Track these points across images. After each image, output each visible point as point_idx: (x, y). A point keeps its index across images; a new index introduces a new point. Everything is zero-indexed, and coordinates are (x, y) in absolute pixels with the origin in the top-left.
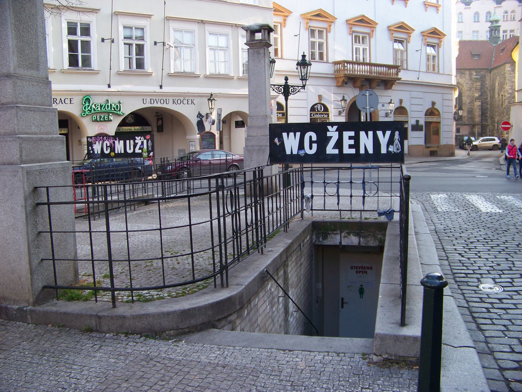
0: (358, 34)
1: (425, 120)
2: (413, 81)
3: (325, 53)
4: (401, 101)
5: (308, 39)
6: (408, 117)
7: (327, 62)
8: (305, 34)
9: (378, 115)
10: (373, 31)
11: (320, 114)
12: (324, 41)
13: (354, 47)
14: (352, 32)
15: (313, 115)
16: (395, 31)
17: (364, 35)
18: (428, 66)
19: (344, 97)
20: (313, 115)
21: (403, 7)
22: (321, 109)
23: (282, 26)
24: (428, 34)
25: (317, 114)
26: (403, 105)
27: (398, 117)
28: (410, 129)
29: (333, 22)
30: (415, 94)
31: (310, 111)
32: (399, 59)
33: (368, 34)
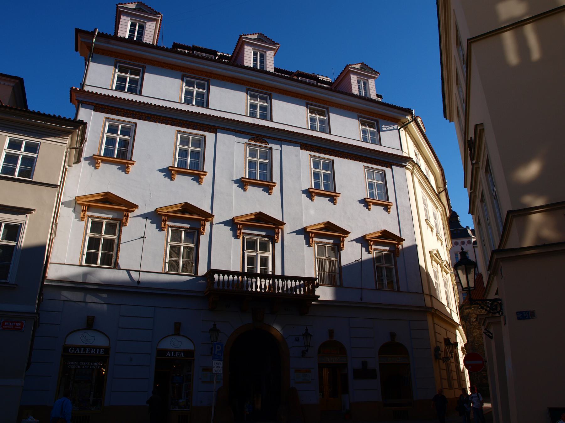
4: (331, 333)
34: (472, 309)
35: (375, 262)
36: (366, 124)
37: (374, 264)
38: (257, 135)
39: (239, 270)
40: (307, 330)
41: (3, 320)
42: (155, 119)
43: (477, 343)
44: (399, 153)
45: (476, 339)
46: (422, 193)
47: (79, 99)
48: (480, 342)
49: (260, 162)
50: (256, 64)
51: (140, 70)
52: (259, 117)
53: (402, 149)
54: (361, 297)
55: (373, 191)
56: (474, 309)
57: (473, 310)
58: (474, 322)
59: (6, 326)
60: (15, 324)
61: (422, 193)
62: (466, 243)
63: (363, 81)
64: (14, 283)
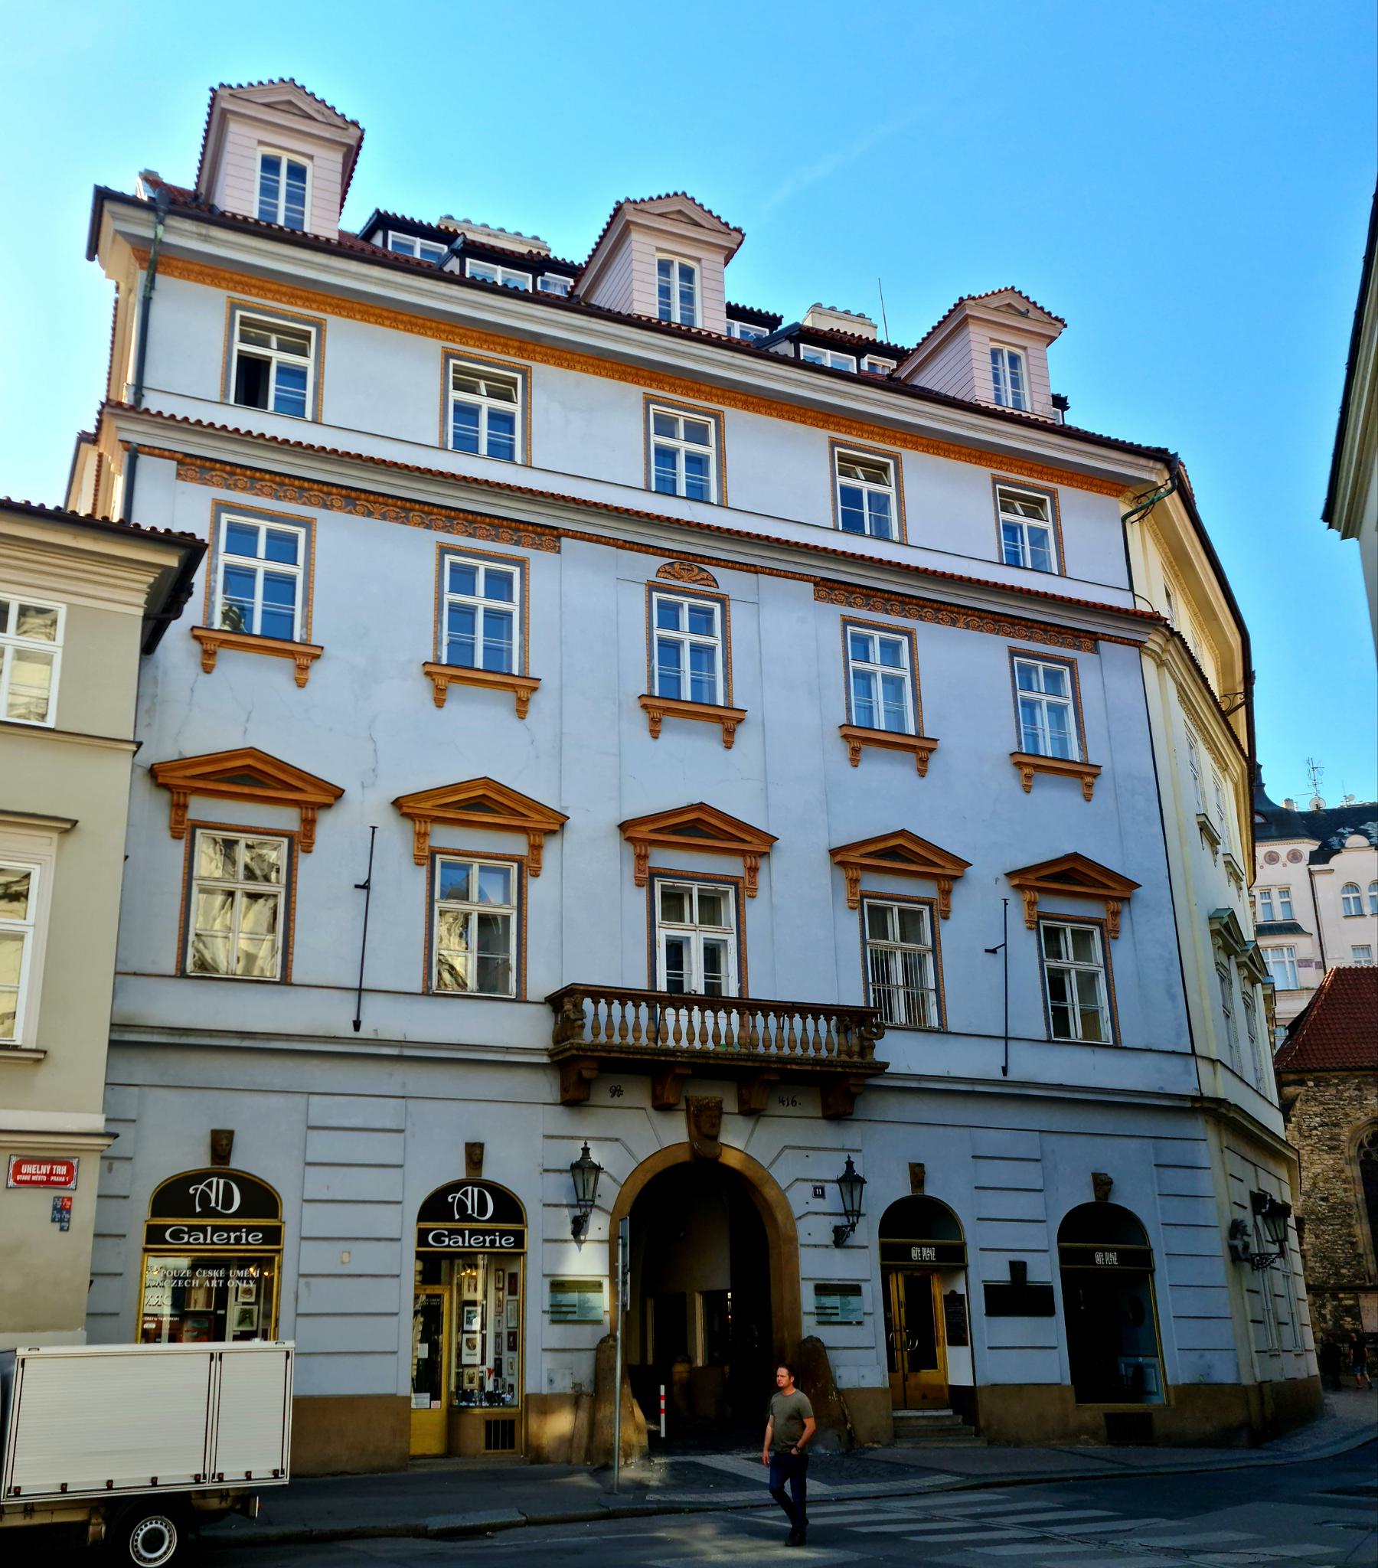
2: (508, 1050)
4: (917, 1174)
5: (1037, 960)
7: (521, 999)
8: (1026, 947)
9: (793, 1240)
13: (662, 935)
14: (647, 877)
15: (437, 1238)
20: (438, 1238)
22: (483, 1209)
23: (527, 873)
24: (1038, 879)
26: (929, 1191)
28: (977, 1303)
29: (765, 854)
31: (422, 1217)
33: (735, 882)
34: (1307, 1086)
35: (1044, 956)
36: (1017, 504)
37: (1042, 962)
39: (641, 983)
40: (850, 1164)
41: (14, 1160)
42: (369, 506)
43: (1323, 1199)
45: (1321, 1184)
46: (1214, 771)
47: (130, 439)
48: (1335, 1194)
49: (244, 320)
50: (669, 305)
52: (684, 494)
54: (1004, 1065)
55: (1035, 729)
56: (1315, 1086)
57: (1311, 1087)
58: (1315, 1128)
59: (26, 1174)
60: (52, 1169)
61: (1214, 771)
64: (34, 1046)
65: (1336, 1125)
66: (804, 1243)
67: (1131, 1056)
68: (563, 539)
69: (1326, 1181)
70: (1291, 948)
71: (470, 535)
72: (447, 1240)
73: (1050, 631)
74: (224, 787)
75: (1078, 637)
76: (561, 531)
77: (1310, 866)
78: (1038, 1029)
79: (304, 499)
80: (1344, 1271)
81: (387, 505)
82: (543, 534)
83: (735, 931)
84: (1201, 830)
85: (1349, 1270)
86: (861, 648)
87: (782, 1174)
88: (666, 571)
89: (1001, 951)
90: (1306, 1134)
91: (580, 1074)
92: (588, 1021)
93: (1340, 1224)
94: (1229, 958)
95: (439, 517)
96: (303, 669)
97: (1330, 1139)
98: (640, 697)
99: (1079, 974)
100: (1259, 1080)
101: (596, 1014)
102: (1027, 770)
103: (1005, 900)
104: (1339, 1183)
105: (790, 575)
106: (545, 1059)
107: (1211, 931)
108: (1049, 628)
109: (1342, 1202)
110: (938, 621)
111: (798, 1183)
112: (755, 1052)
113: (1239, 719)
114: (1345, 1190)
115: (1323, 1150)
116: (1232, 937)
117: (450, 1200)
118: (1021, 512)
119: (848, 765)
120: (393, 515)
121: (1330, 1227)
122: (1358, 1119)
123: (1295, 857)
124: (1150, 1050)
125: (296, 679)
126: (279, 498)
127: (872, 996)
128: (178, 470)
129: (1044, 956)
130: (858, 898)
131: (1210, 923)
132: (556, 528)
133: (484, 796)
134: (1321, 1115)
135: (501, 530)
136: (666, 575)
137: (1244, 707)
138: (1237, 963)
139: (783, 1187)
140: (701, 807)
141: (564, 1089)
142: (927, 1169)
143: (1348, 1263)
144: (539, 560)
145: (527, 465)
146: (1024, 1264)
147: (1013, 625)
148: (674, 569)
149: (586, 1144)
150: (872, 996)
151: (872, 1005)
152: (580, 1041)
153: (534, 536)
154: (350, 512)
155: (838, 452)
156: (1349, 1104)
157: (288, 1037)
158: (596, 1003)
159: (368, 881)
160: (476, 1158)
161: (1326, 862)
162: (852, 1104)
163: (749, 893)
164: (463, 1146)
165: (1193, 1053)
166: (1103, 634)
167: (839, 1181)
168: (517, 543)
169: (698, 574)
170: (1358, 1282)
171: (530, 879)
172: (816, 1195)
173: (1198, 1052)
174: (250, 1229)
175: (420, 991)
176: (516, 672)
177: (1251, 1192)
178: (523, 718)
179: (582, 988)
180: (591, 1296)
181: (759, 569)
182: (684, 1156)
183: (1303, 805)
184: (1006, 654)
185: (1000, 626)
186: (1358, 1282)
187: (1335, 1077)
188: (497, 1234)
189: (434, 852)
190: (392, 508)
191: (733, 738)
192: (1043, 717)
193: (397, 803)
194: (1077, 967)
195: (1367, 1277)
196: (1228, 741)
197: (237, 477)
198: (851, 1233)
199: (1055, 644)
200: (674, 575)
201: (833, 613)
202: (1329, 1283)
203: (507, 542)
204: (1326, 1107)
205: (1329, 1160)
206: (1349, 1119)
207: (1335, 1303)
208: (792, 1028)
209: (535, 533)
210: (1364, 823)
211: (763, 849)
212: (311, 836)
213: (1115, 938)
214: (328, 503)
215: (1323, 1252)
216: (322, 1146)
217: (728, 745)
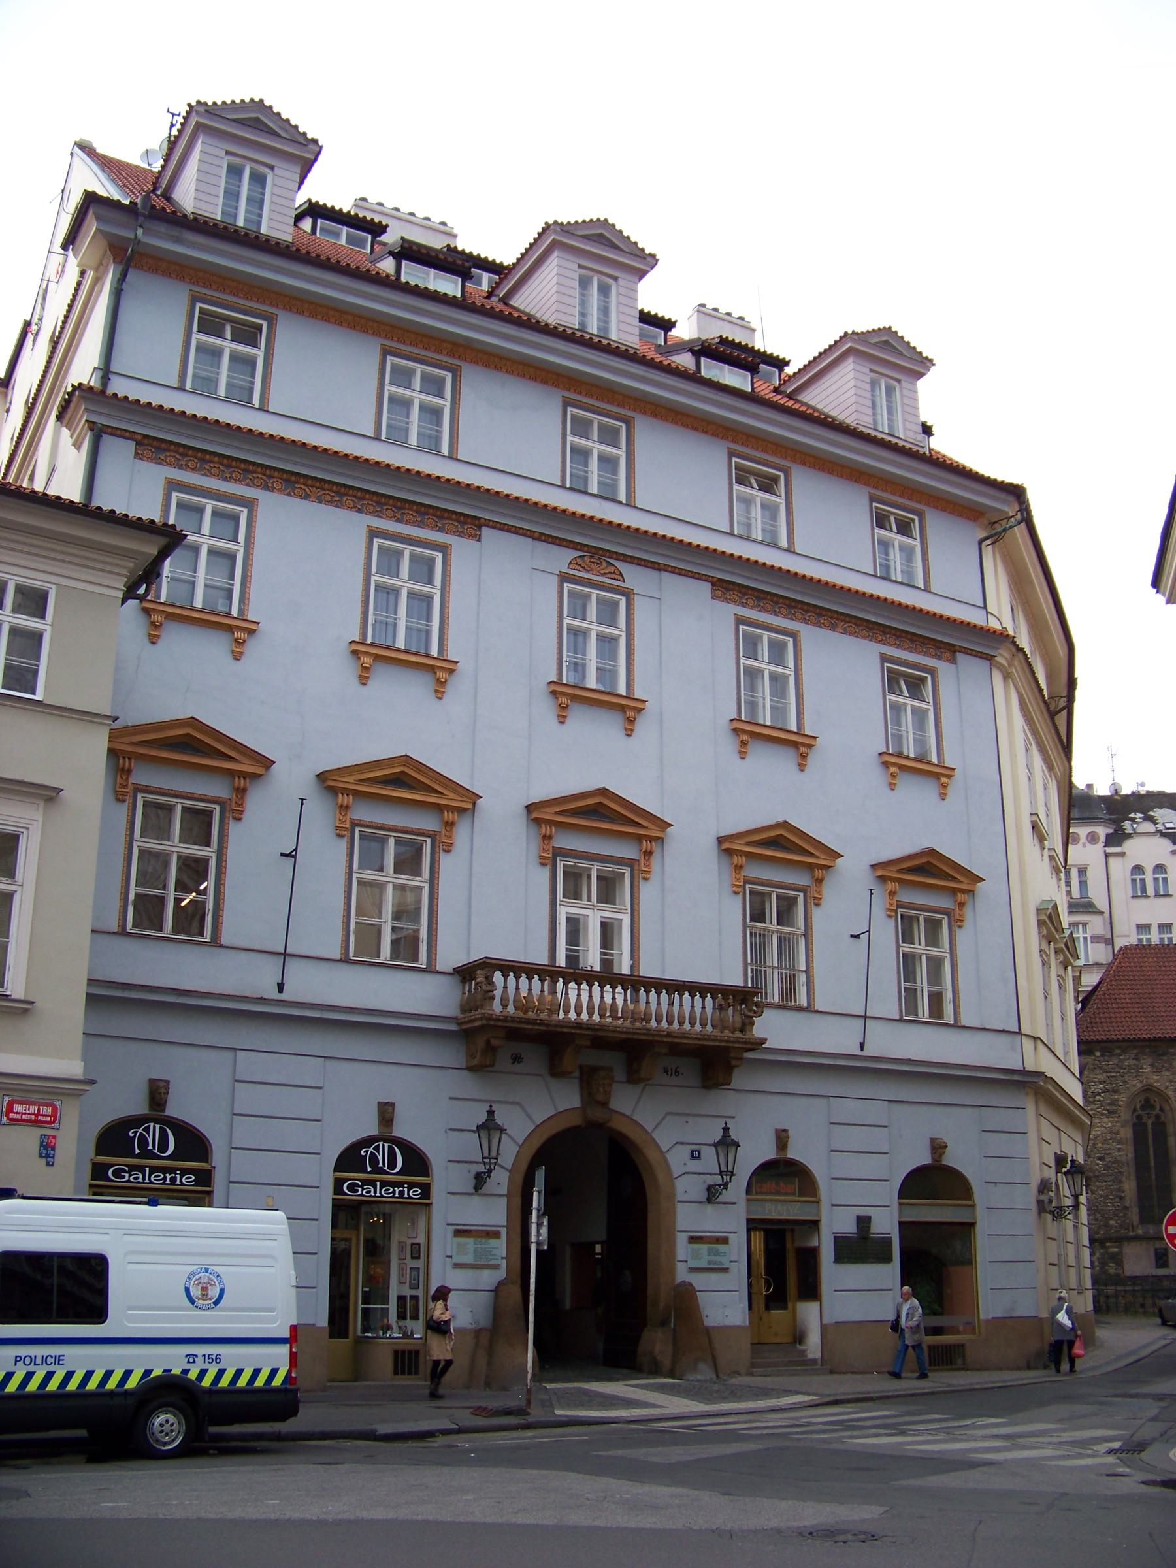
0: (582, 864)
1: (748, 1212)
3: (948, 995)
4: (782, 1139)
6: (818, 1202)
7: (431, 970)
8: (885, 932)
9: (671, 1197)
10: (648, 854)
11: (384, 1184)
12: (943, 951)
13: (562, 913)
14: (549, 859)
15: (352, 1188)
16: (357, 794)
17: (608, 867)
18: (910, 997)
19: (491, 1113)
20: (352, 1188)
21: (794, 768)
22: (392, 1164)
25: (372, 1183)
26: (792, 1154)
27: (768, 1205)
30: (847, 1109)
31: (338, 1167)
32: (773, 968)
33: (630, 863)
34: (1095, 1055)
37: (898, 946)
38: (593, 550)
39: (543, 959)
41: (7, 1099)
42: (307, 490)
43: (1100, 1159)
44: (975, 617)
45: (1100, 1145)
51: (262, 325)
53: (985, 607)
56: (1102, 1055)
58: (1099, 1094)
59: (17, 1113)
61: (1025, 732)
62: (1083, 839)
63: (885, 382)
65: (1115, 1092)
66: (680, 1199)
67: (967, 1034)
68: (484, 529)
69: (1105, 1142)
70: (1085, 925)
71: (398, 520)
72: (360, 1189)
73: (916, 641)
74: (165, 754)
75: (939, 648)
76: (482, 521)
77: (1106, 849)
78: (891, 1008)
79: (248, 480)
80: (1112, 1222)
81: (323, 489)
82: (465, 523)
83: (629, 911)
84: (1033, 828)
85: (1116, 1221)
86: (752, 645)
87: (664, 1138)
88: (577, 564)
89: (864, 937)
90: (1091, 1099)
91: (488, 1042)
92: (498, 994)
93: (1113, 1181)
94: (1049, 945)
95: (370, 502)
96: (240, 643)
97: (1110, 1104)
98: (549, 683)
99: (928, 958)
100: (1066, 1053)
101: (505, 987)
102: (893, 769)
103: (871, 890)
104: (1114, 1144)
105: (690, 574)
106: (453, 1027)
107: (1038, 921)
108: (915, 638)
109: (1116, 1161)
110: (820, 625)
111: (677, 1146)
112: (648, 1026)
113: (1061, 719)
114: (1119, 1150)
115: (1102, 1114)
116: (1053, 924)
117: (363, 1153)
118: (895, 529)
119: (736, 756)
120: (329, 499)
121: (1104, 1184)
122: (1135, 1086)
123: (1093, 838)
124: (984, 1029)
125: (233, 652)
126: (226, 479)
127: (750, 975)
128: (136, 448)
129: (901, 942)
130: (742, 884)
131: (1038, 913)
132: (479, 518)
133: (403, 772)
134: (1105, 1082)
135: (427, 517)
136: (577, 567)
137: (1065, 711)
138: (1055, 948)
139: (664, 1150)
140: (604, 792)
141: (471, 1055)
142: (790, 1133)
143: (1116, 1215)
144: (461, 547)
145: (452, 457)
146: (870, 1217)
147: (884, 633)
148: (584, 562)
149: (491, 1106)
150: (750, 975)
151: (750, 985)
152: (490, 1012)
153: (456, 524)
154: (289, 494)
155: (735, 462)
156: (1128, 1072)
157: (220, 996)
158: (505, 976)
159: (296, 850)
160: (388, 1116)
161: (1119, 844)
162: (730, 1075)
163: (644, 875)
164: (376, 1104)
165: (1019, 1033)
166: (960, 647)
167: (716, 1145)
168: (441, 530)
169: (606, 568)
170: (1122, 1231)
171: (443, 855)
172: (693, 1157)
173: (1023, 1031)
174: (184, 1172)
175: (338, 957)
176: (434, 652)
177: (1056, 1153)
178: (440, 698)
179: (494, 962)
180: (493, 1242)
181: (662, 566)
182: (576, 1121)
183: (1102, 790)
184: (878, 660)
185: (873, 633)
186: (1122, 1231)
187: (1119, 1047)
188: (406, 1186)
189: (355, 824)
190: (327, 492)
191: (633, 726)
192: (908, 719)
193: (322, 777)
194: (927, 952)
195: (1130, 1228)
196: (1056, 745)
197: (188, 458)
198: (724, 1190)
199: (920, 653)
200: (584, 568)
201: (728, 611)
202: (1099, 1233)
203: (432, 528)
204: (1108, 1074)
205: (1108, 1123)
206: (1127, 1086)
207: (1102, 1251)
208: (681, 1005)
209: (458, 521)
210: (1152, 809)
211: (659, 834)
212: (242, 804)
213: (646, 879)
214: (269, 485)
215: (1097, 1206)
216: (247, 1099)
217: (629, 733)
